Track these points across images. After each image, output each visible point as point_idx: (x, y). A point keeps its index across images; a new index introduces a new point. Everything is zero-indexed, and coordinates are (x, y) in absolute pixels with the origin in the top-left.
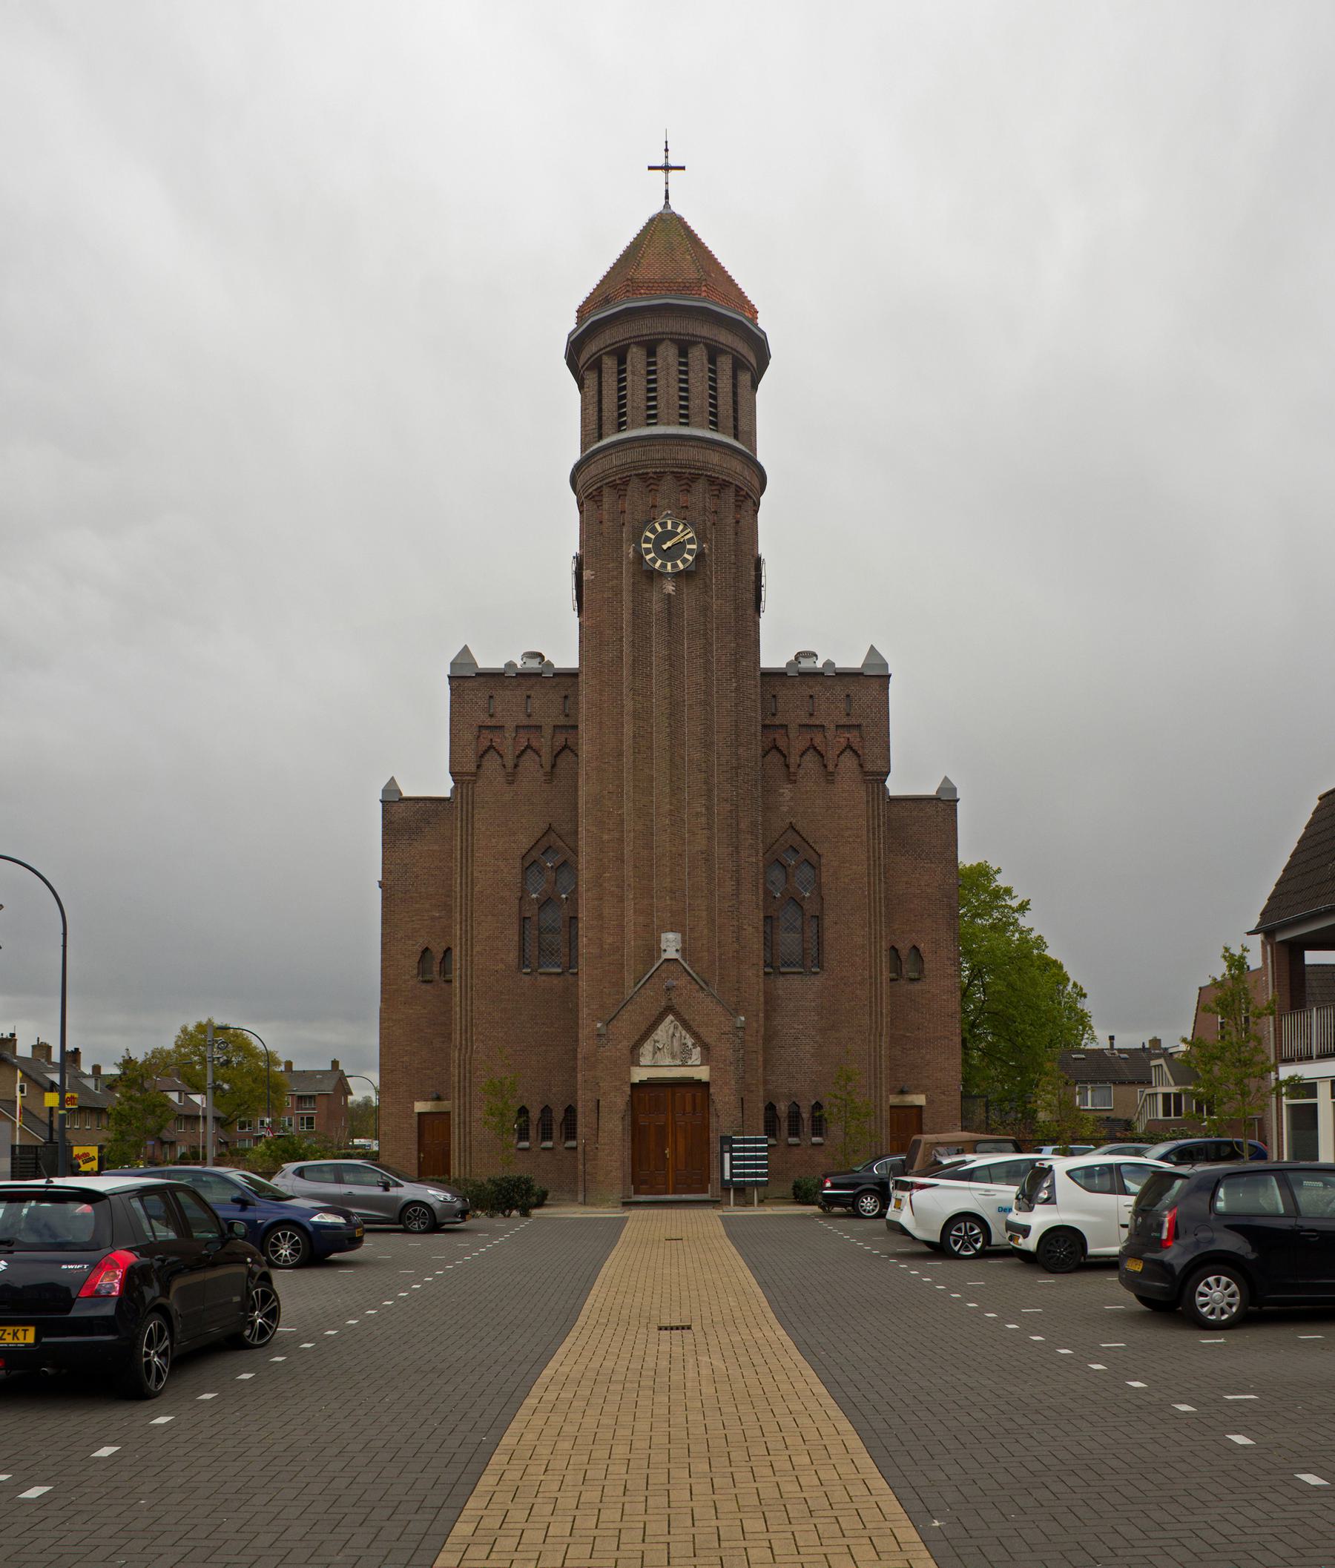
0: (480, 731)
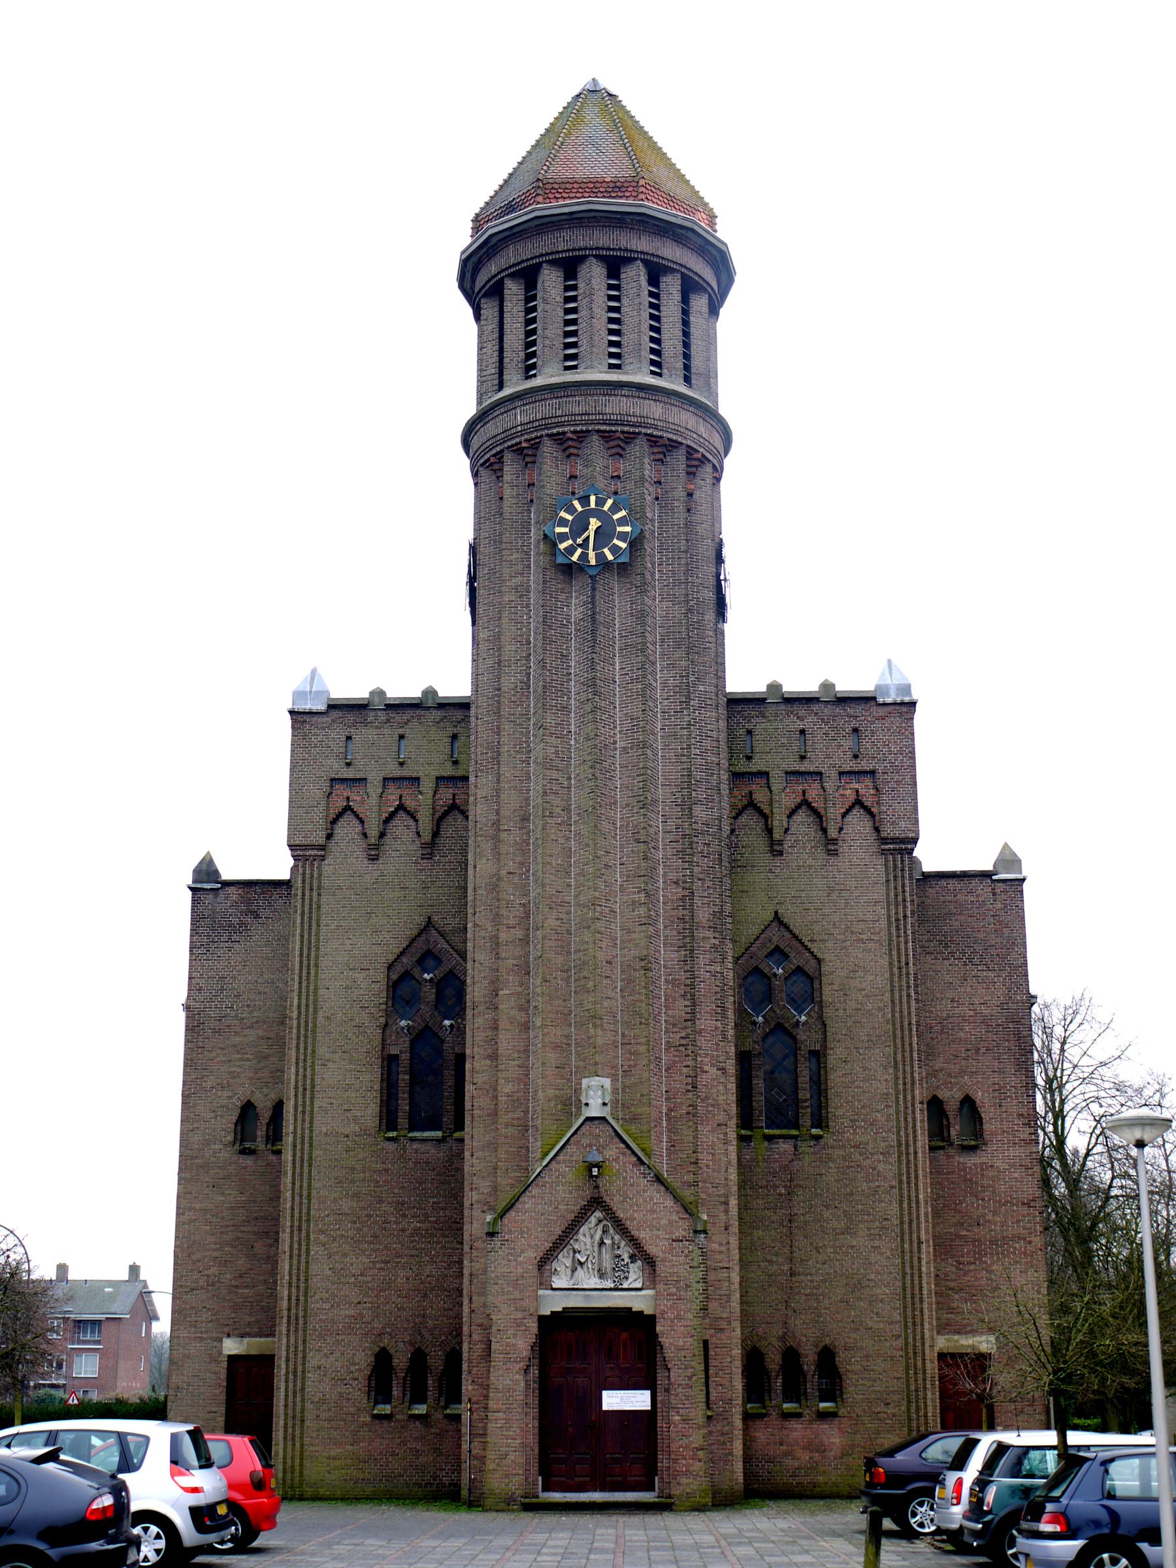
0: (332, 786)
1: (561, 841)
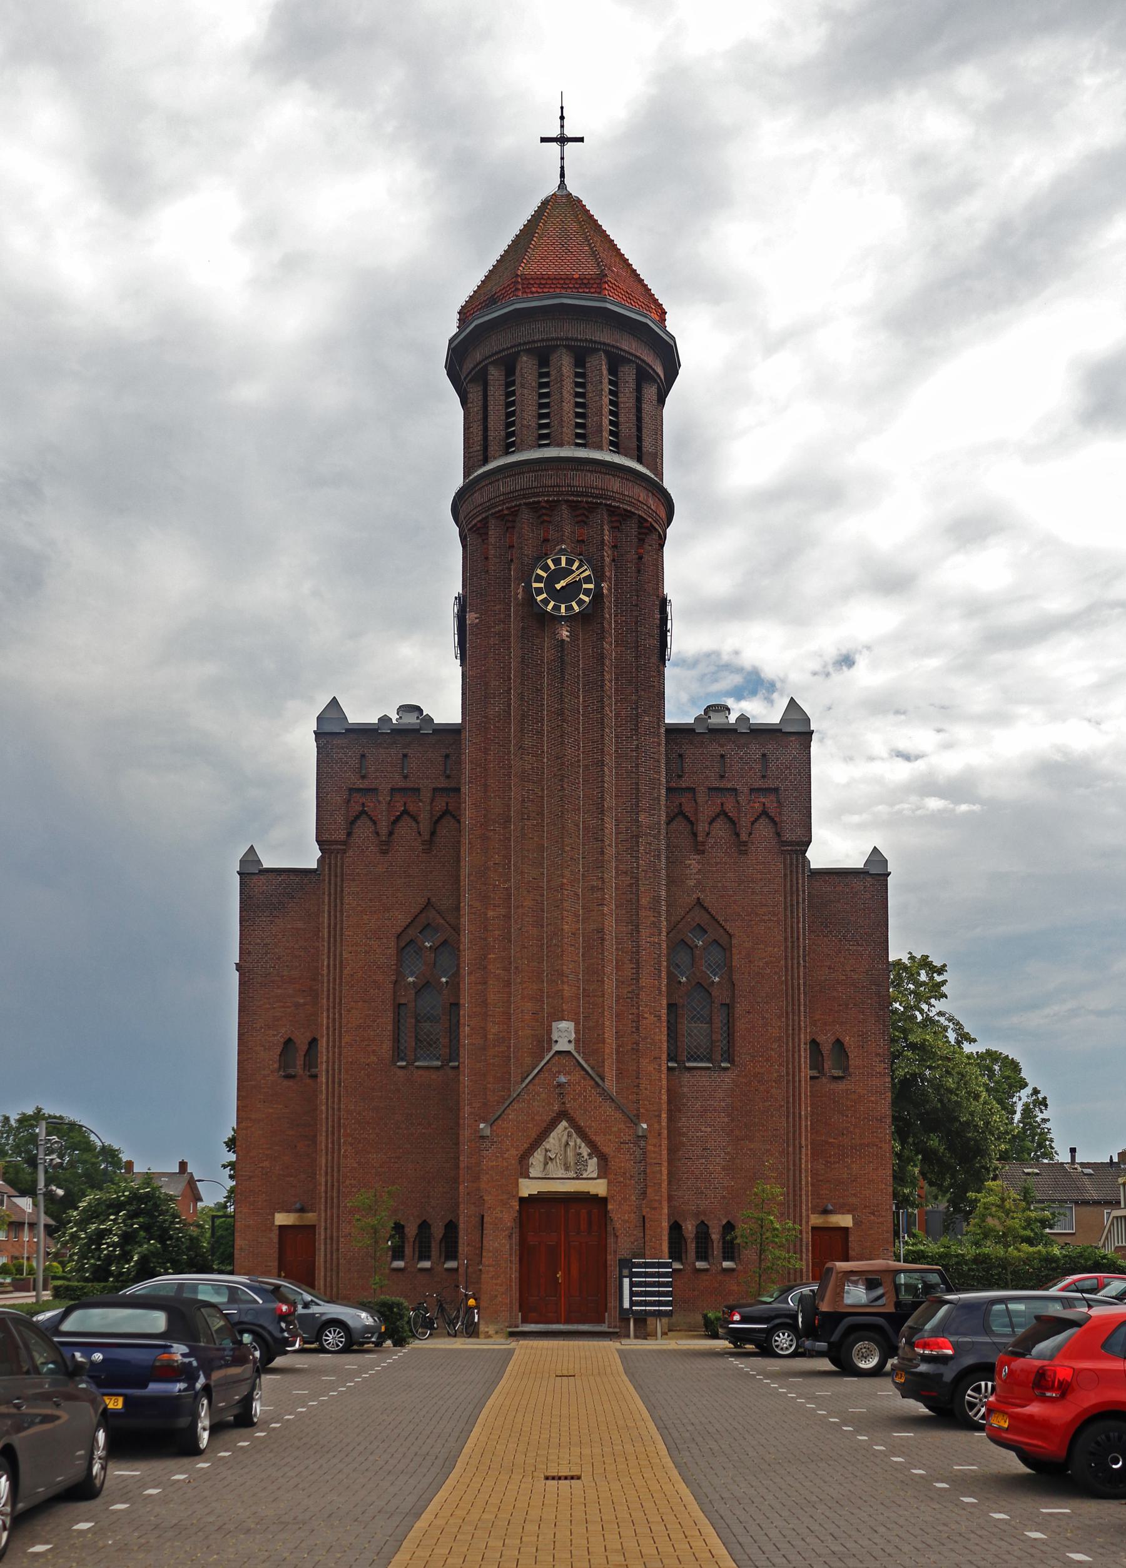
0: (350, 794)
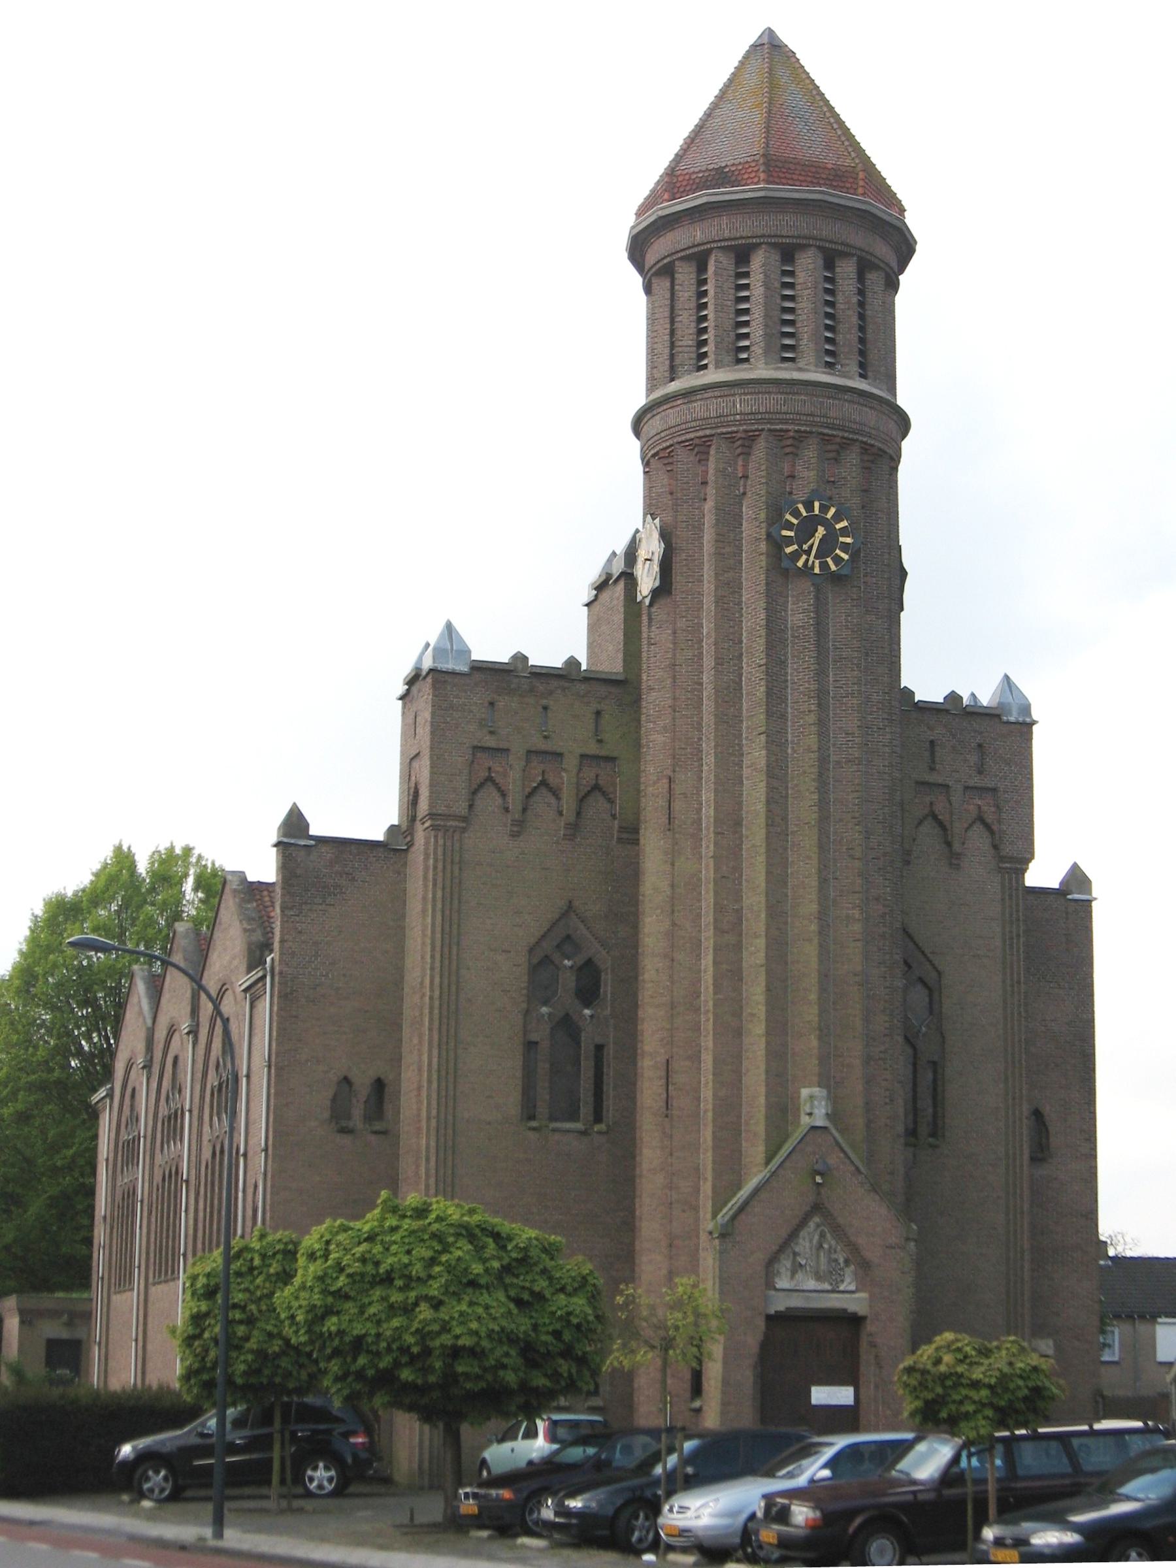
0: (474, 754)
1: (780, 851)
